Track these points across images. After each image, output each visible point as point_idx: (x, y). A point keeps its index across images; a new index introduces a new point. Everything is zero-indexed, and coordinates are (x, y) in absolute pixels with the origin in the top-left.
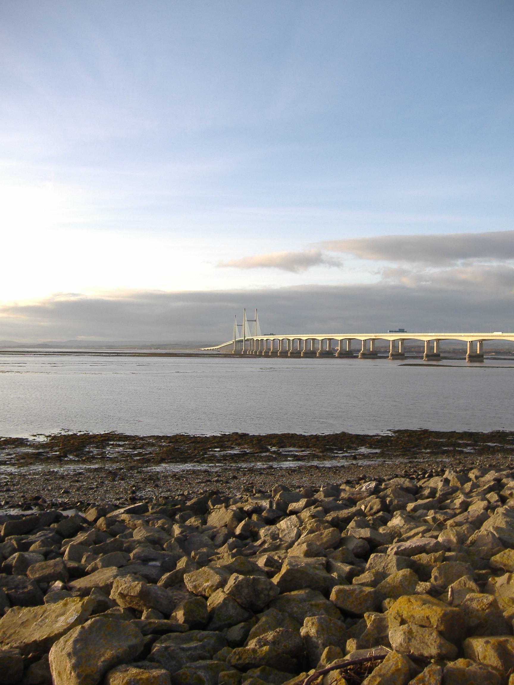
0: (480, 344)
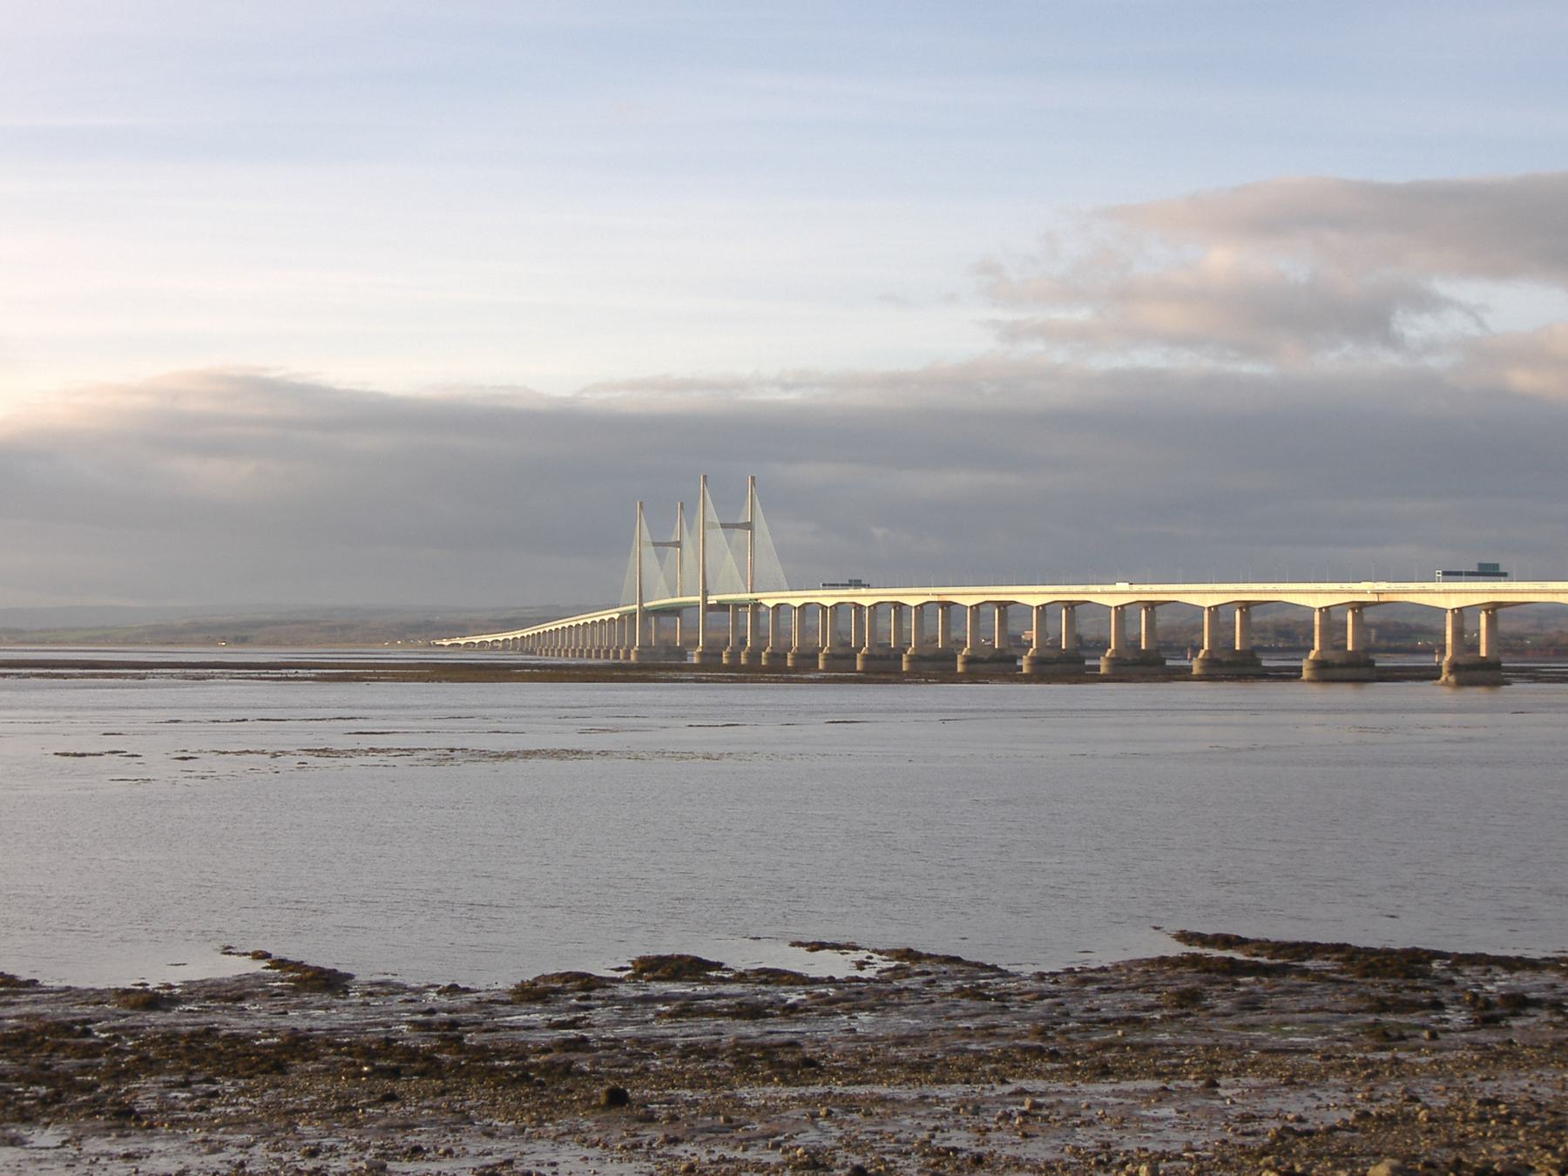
0: (1488, 617)
